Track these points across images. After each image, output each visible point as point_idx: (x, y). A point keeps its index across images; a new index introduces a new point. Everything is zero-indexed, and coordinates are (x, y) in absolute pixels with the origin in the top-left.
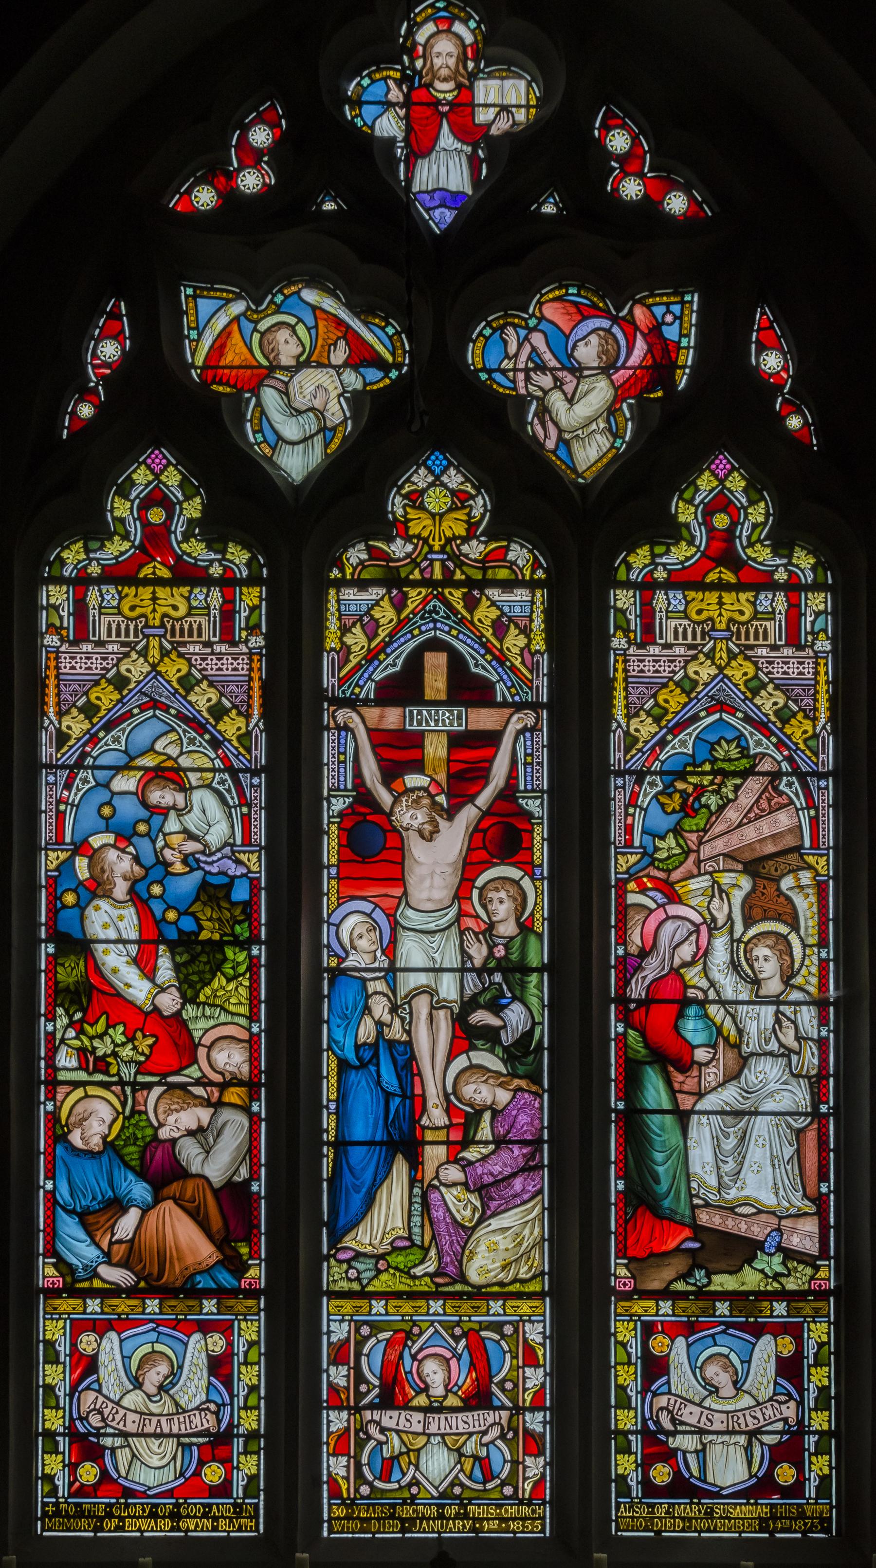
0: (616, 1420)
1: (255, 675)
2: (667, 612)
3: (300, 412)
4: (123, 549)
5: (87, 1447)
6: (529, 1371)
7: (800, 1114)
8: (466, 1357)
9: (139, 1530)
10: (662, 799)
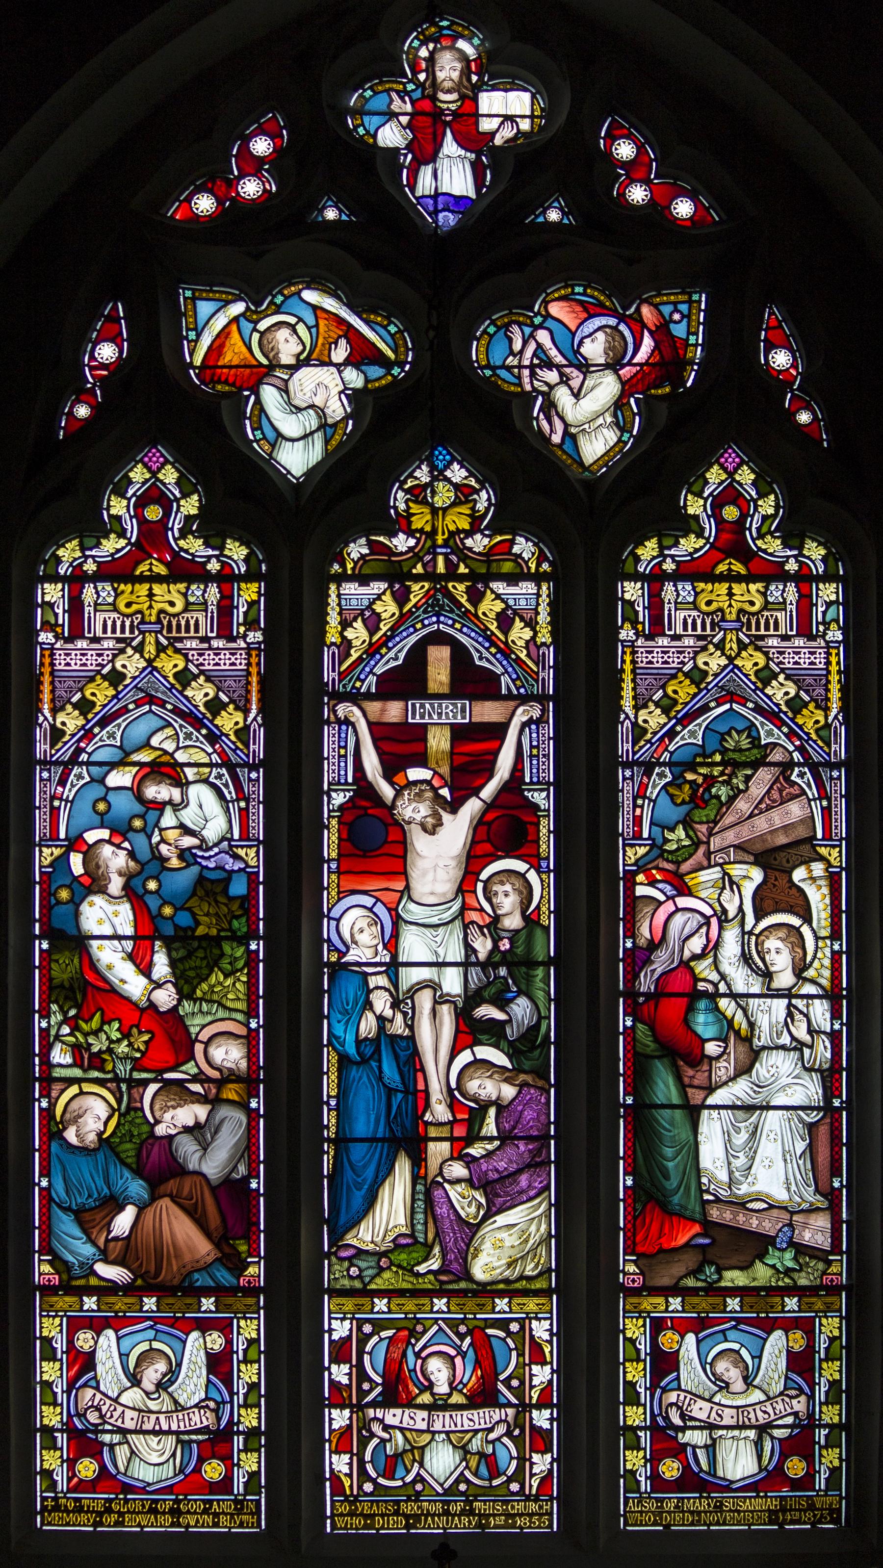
0: (625, 1417)
1: (254, 670)
2: (676, 603)
3: (299, 409)
4: (119, 546)
5: (84, 1442)
6: (536, 1369)
7: (812, 1108)
8: (471, 1354)
9: (139, 1525)
10: (671, 790)
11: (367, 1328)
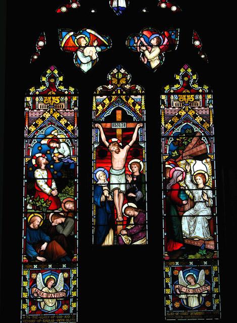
3: (86, 57)
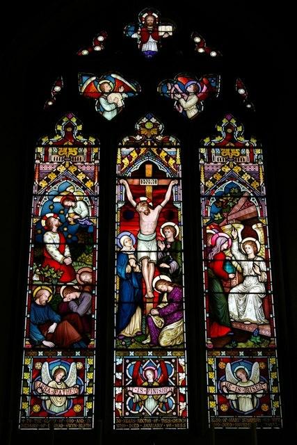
1: (96, 171)
5: (37, 399)
6: (180, 374)
11: (127, 361)
